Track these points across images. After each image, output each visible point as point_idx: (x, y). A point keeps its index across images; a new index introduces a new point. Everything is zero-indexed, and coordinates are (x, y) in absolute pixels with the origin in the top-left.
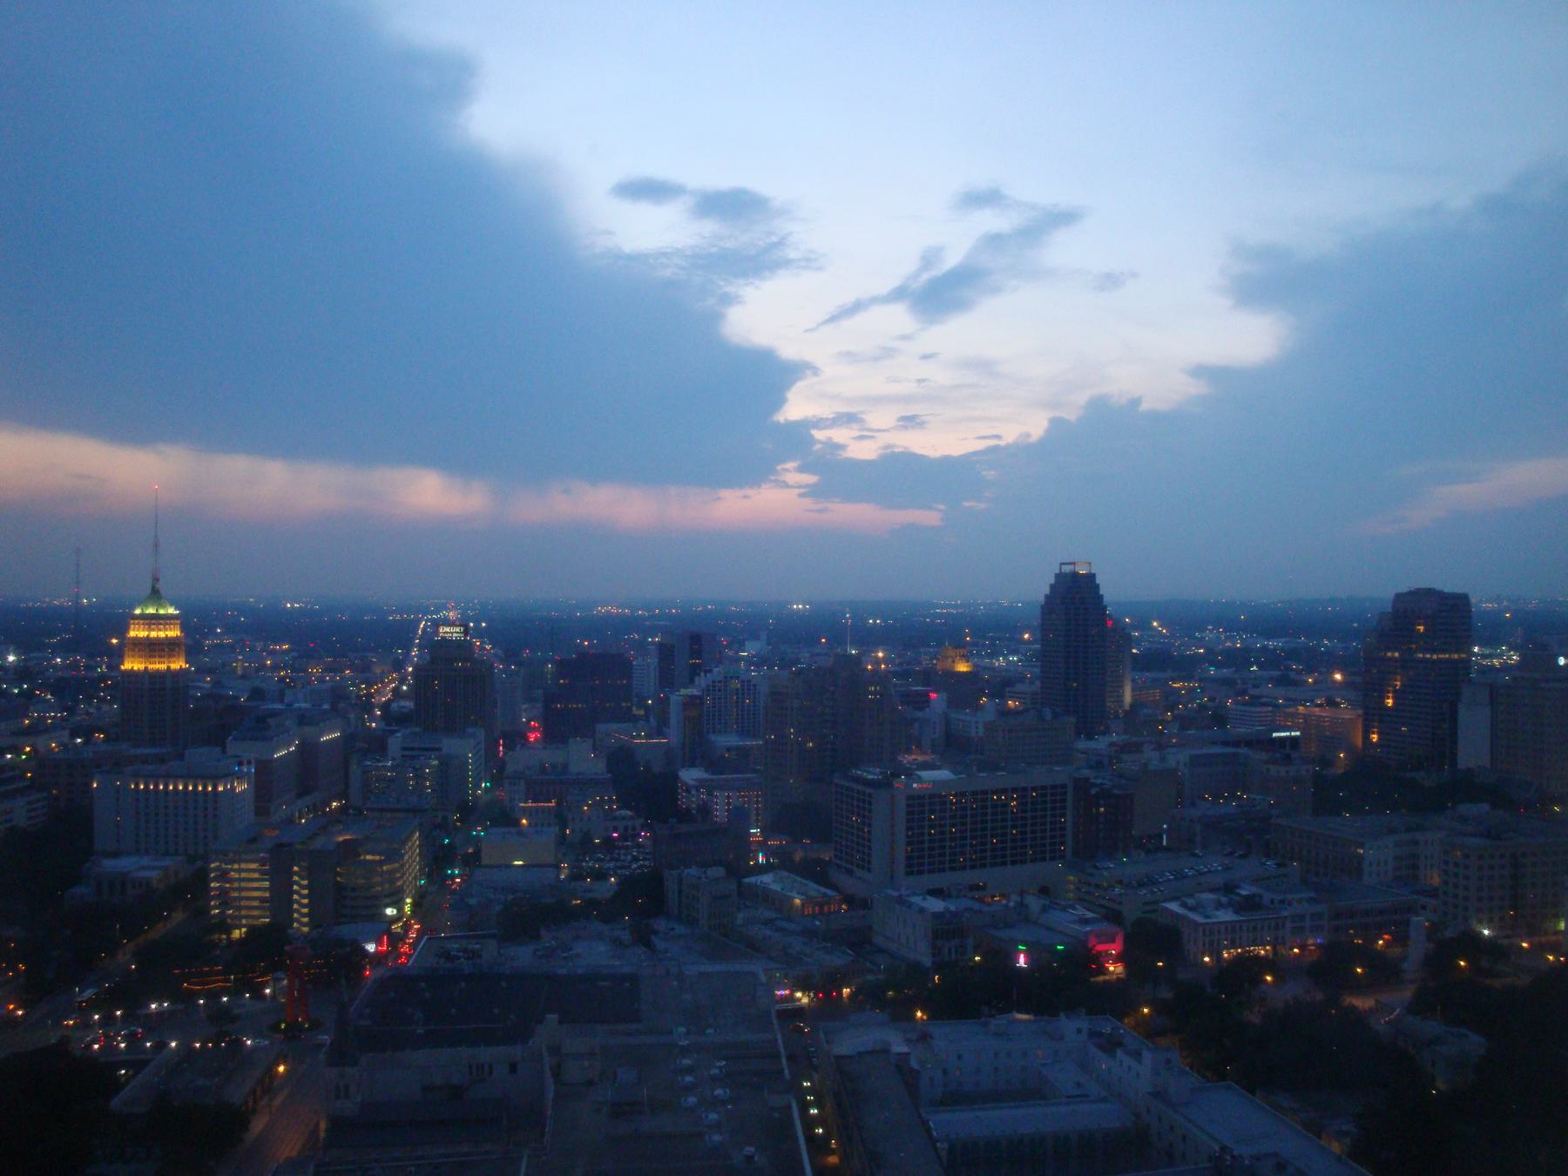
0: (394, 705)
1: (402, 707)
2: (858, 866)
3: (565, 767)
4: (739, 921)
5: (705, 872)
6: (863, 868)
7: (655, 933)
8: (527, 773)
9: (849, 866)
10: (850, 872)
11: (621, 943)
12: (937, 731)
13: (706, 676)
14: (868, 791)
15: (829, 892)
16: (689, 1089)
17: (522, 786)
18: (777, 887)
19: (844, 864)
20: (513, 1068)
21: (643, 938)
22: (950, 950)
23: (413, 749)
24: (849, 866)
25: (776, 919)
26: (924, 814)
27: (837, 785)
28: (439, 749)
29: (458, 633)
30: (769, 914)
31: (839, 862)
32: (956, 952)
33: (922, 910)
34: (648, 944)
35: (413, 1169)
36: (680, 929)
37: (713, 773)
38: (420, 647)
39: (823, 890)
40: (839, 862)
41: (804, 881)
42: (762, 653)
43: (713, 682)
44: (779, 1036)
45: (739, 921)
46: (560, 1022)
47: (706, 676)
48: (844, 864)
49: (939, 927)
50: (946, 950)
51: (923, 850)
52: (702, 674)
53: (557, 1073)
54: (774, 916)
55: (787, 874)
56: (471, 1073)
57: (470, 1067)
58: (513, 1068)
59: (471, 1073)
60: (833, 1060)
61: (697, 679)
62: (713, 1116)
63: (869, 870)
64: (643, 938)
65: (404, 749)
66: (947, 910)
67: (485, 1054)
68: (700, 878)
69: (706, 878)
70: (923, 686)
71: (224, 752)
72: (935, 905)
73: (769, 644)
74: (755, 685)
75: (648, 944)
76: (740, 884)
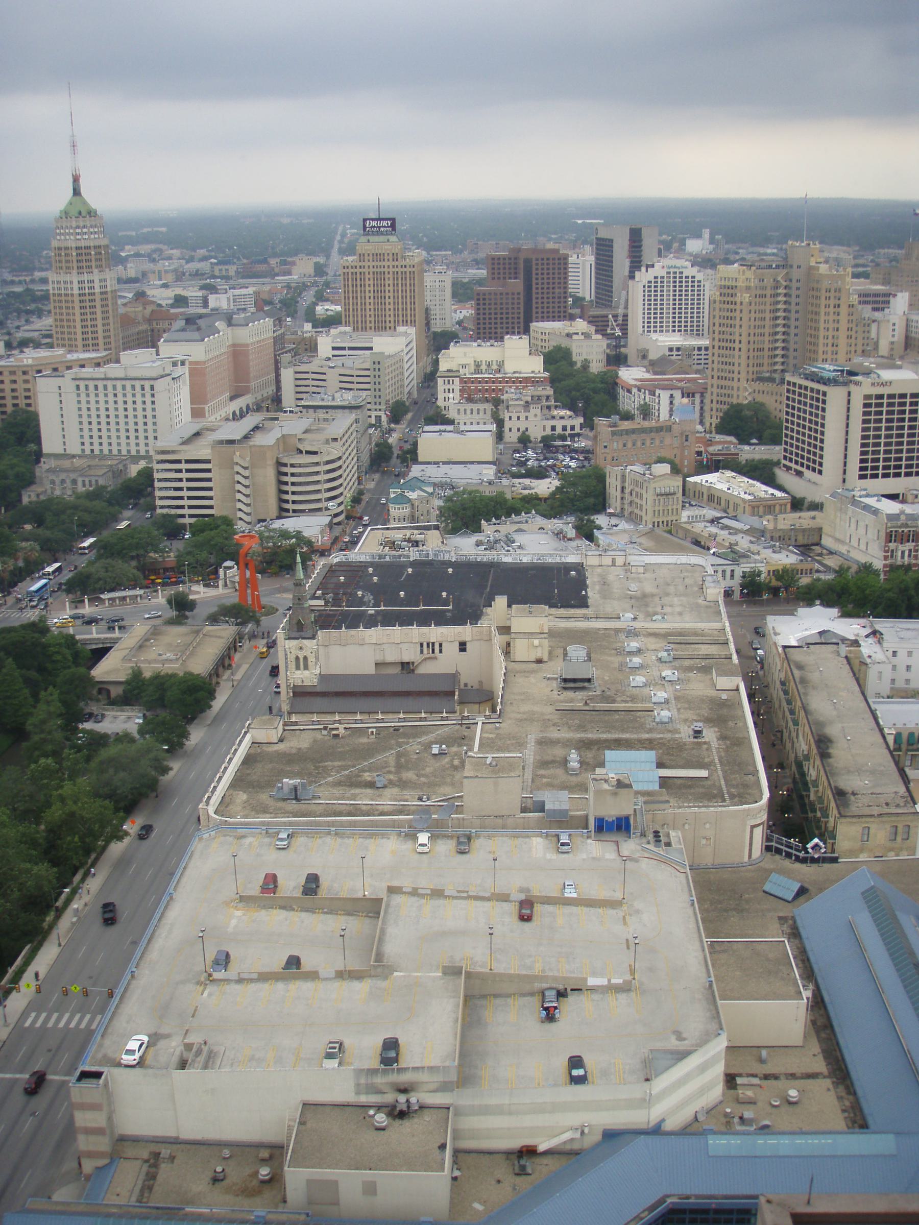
0: (319, 309)
1: (327, 310)
2: (808, 467)
3: (501, 365)
4: (684, 519)
5: (649, 469)
6: (814, 470)
7: (599, 528)
8: (462, 371)
9: (799, 468)
10: (799, 474)
11: (564, 537)
12: (896, 333)
13: (647, 271)
14: (822, 388)
15: (779, 494)
16: (635, 670)
17: (457, 385)
18: (724, 487)
19: (793, 465)
20: (463, 647)
21: (587, 533)
22: (903, 552)
23: (343, 349)
24: (799, 468)
25: (722, 518)
26: (887, 411)
27: (789, 383)
28: (371, 349)
29: (385, 227)
30: (711, 513)
31: (787, 463)
32: (909, 556)
33: (876, 512)
34: (590, 537)
35: (374, 730)
36: (623, 525)
37: (655, 373)
38: (311, 578)
39: (771, 491)
40: (787, 463)
41: (751, 481)
42: (704, 252)
43: (656, 278)
44: (727, 624)
45: (684, 519)
46: (509, 606)
47: (647, 271)
48: (793, 465)
49: (894, 529)
50: (899, 554)
51: (878, 452)
52: (643, 269)
53: (507, 652)
54: (719, 515)
55: (734, 474)
56: (422, 652)
57: (422, 645)
58: (463, 647)
59: (422, 652)
60: (780, 650)
61: (637, 274)
62: (661, 695)
63: (820, 472)
64: (587, 533)
65: (334, 348)
66: (902, 512)
67: (435, 633)
68: (644, 474)
69: (650, 474)
70: (883, 284)
71: (158, 354)
72: (891, 507)
73: (711, 243)
74: (699, 282)
75: (590, 537)
76: (684, 482)
